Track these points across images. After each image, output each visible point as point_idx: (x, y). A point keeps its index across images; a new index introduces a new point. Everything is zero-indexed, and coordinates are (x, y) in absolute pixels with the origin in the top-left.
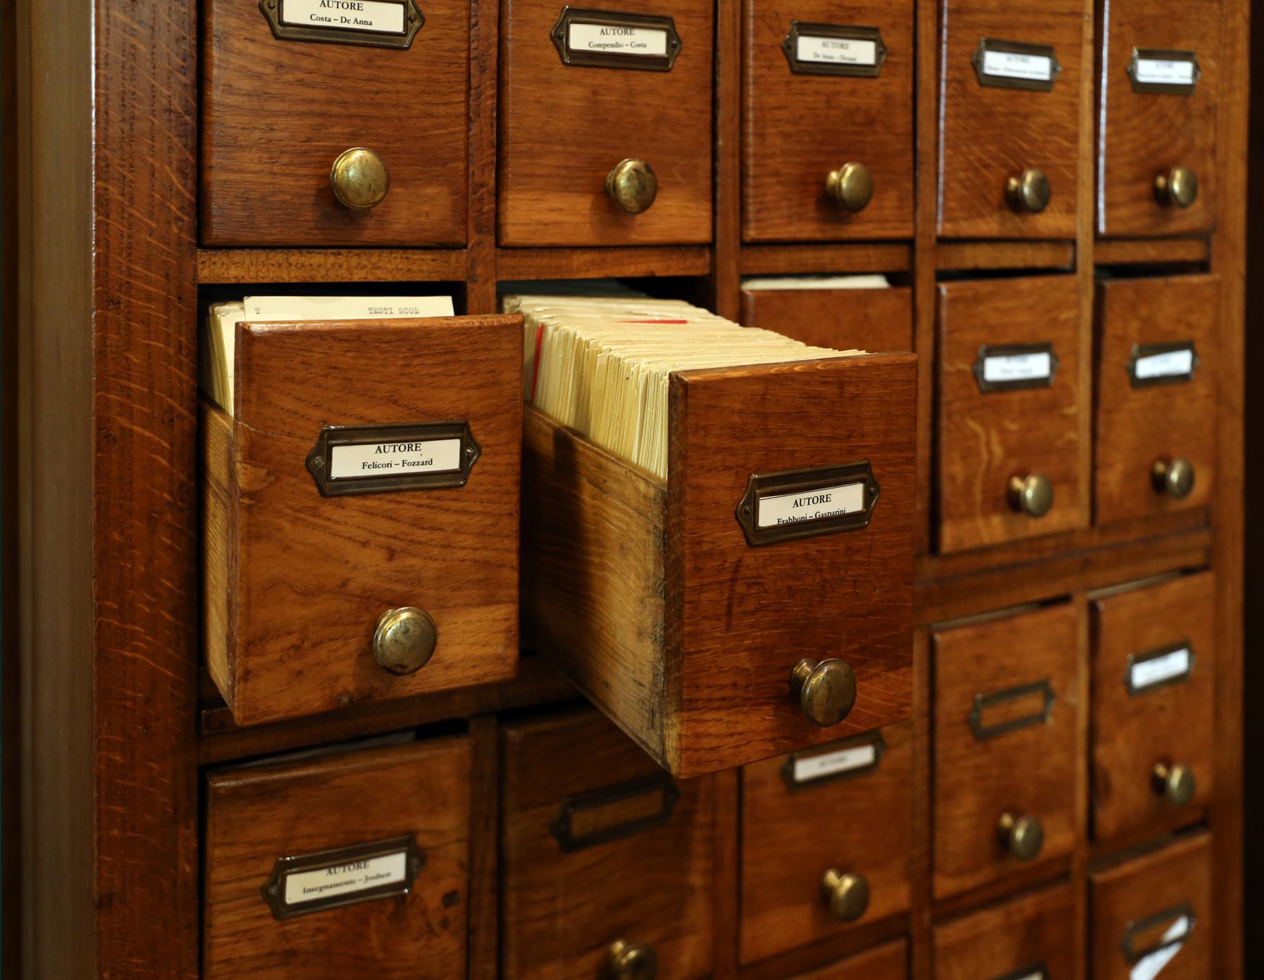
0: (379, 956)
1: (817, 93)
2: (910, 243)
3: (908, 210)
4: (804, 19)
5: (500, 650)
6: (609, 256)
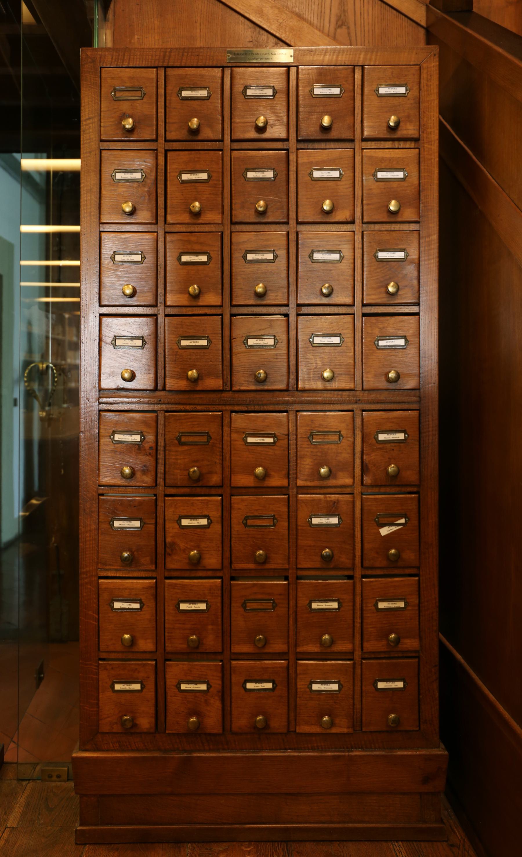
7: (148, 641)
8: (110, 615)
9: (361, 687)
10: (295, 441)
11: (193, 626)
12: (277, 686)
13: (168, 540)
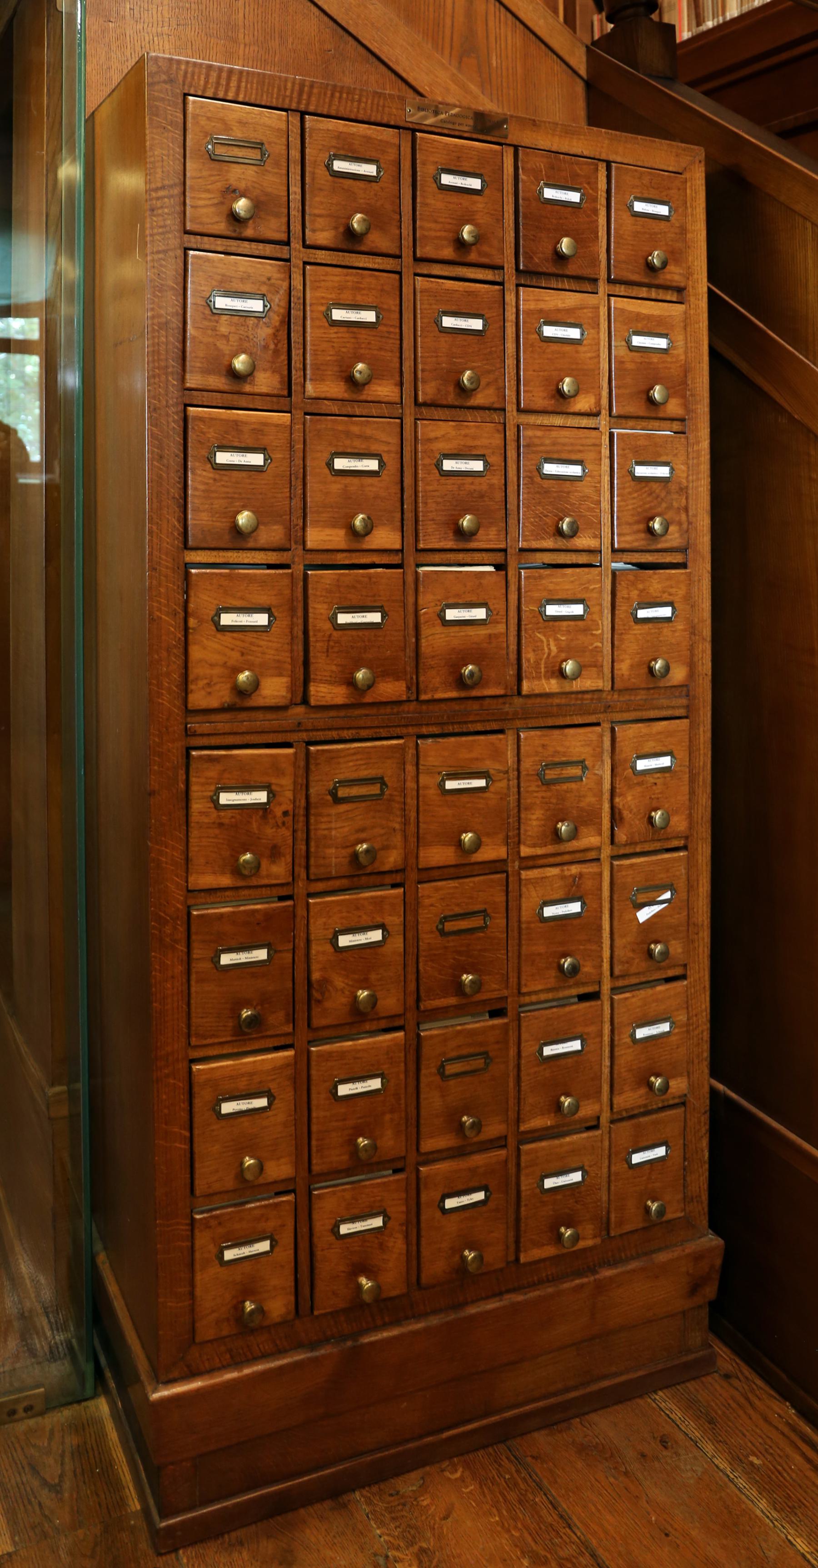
0: (257, 832)
1: (453, 484)
2: (505, 551)
3: (503, 536)
4: (446, 452)
5: (284, 694)
6: (354, 555)
7: (283, 1160)
8: (215, 1127)
9: (609, 1167)
10: (516, 781)
11: (359, 1121)
12: (491, 1194)
13: (316, 976)
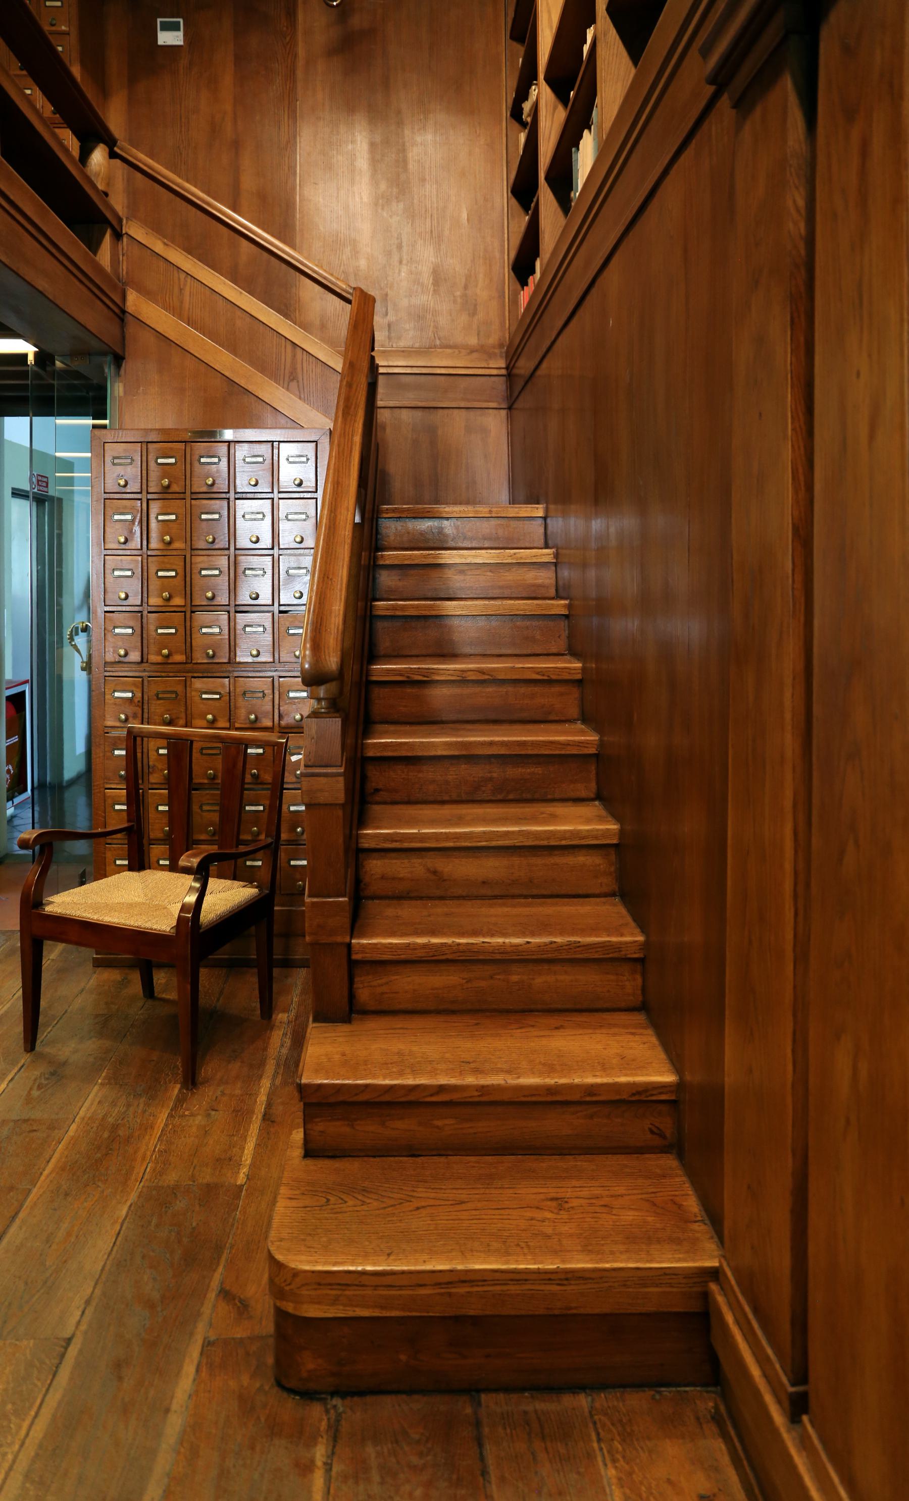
13: (151, 763)
